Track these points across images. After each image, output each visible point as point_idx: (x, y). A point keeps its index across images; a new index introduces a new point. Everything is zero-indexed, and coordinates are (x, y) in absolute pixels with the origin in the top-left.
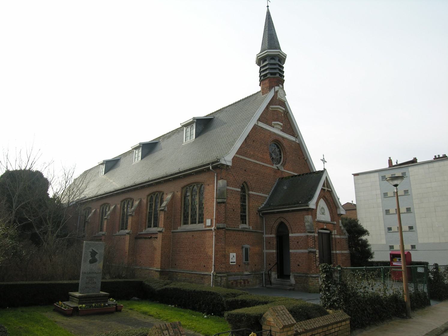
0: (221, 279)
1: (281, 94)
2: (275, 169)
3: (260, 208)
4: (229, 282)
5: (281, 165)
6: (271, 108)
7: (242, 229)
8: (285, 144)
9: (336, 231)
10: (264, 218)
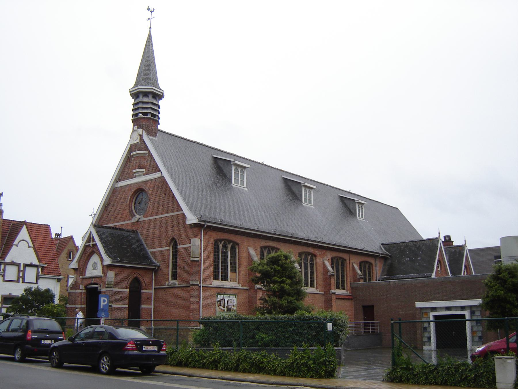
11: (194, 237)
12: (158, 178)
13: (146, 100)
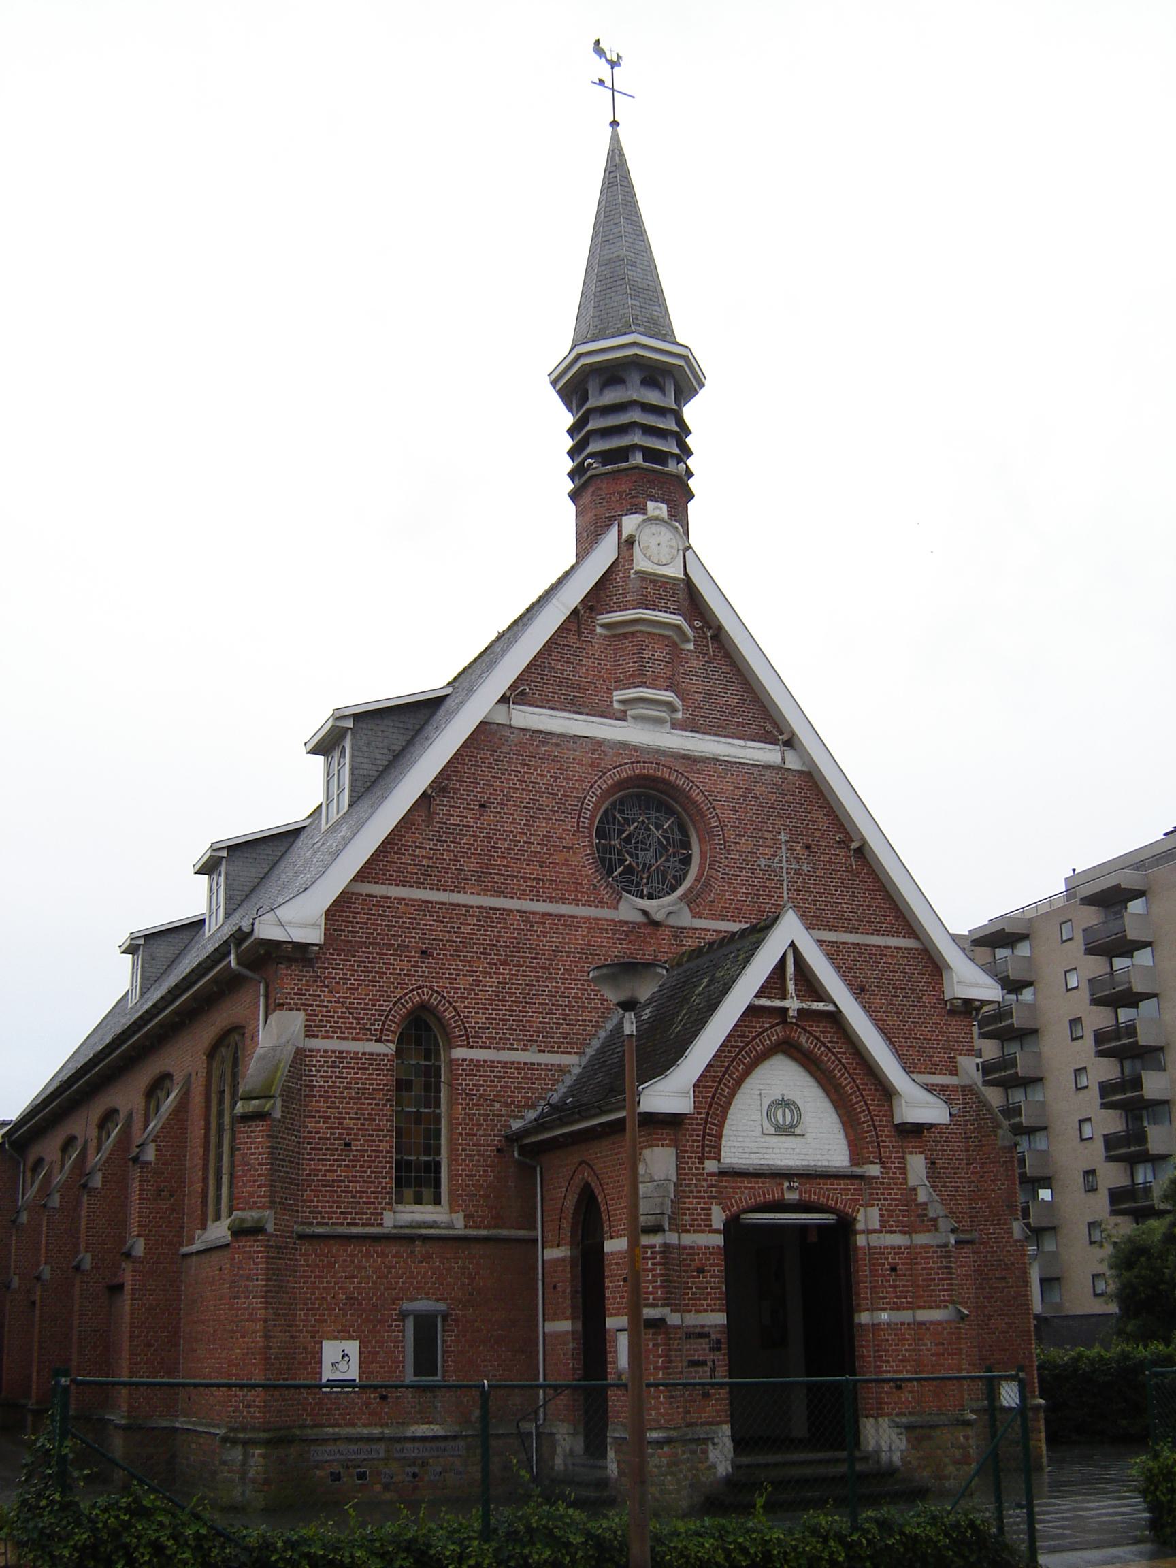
0: (245, 1454)
1: (654, 549)
2: (627, 923)
3: (516, 1125)
4: (317, 1467)
5: (681, 898)
6: (602, 626)
7: (395, 1231)
8: (698, 787)
9: (874, 1213)
10: (538, 1169)
11: (967, 1050)
12: (763, 766)
13: (612, 396)
